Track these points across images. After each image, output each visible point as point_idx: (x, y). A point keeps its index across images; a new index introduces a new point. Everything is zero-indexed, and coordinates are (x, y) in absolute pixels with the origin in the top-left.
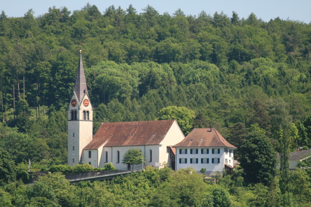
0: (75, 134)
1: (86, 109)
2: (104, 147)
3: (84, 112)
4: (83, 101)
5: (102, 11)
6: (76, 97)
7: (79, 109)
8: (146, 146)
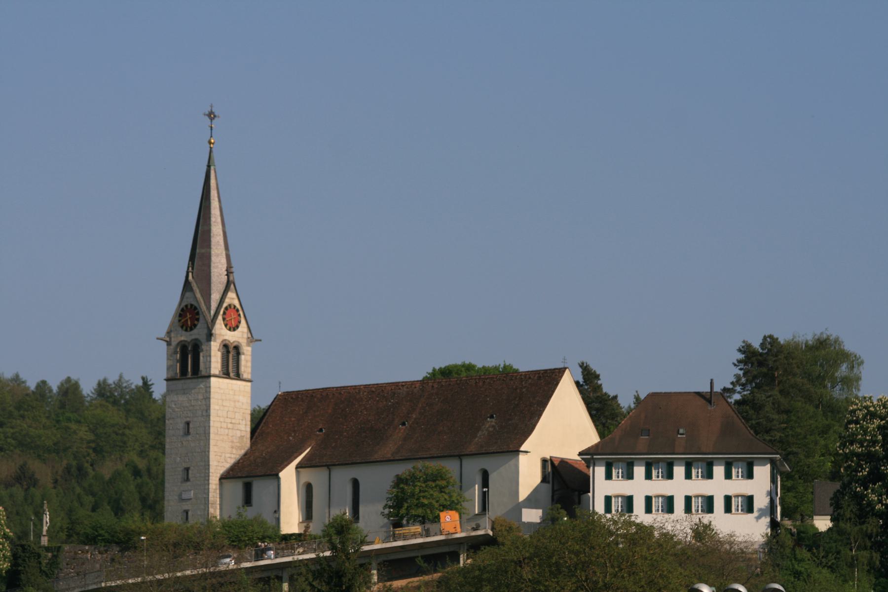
0: (191, 426)
1: (232, 337)
2: (298, 467)
3: (226, 346)
4: (222, 312)
5: (88, 388)
6: (198, 295)
7: (210, 336)
8: (462, 457)
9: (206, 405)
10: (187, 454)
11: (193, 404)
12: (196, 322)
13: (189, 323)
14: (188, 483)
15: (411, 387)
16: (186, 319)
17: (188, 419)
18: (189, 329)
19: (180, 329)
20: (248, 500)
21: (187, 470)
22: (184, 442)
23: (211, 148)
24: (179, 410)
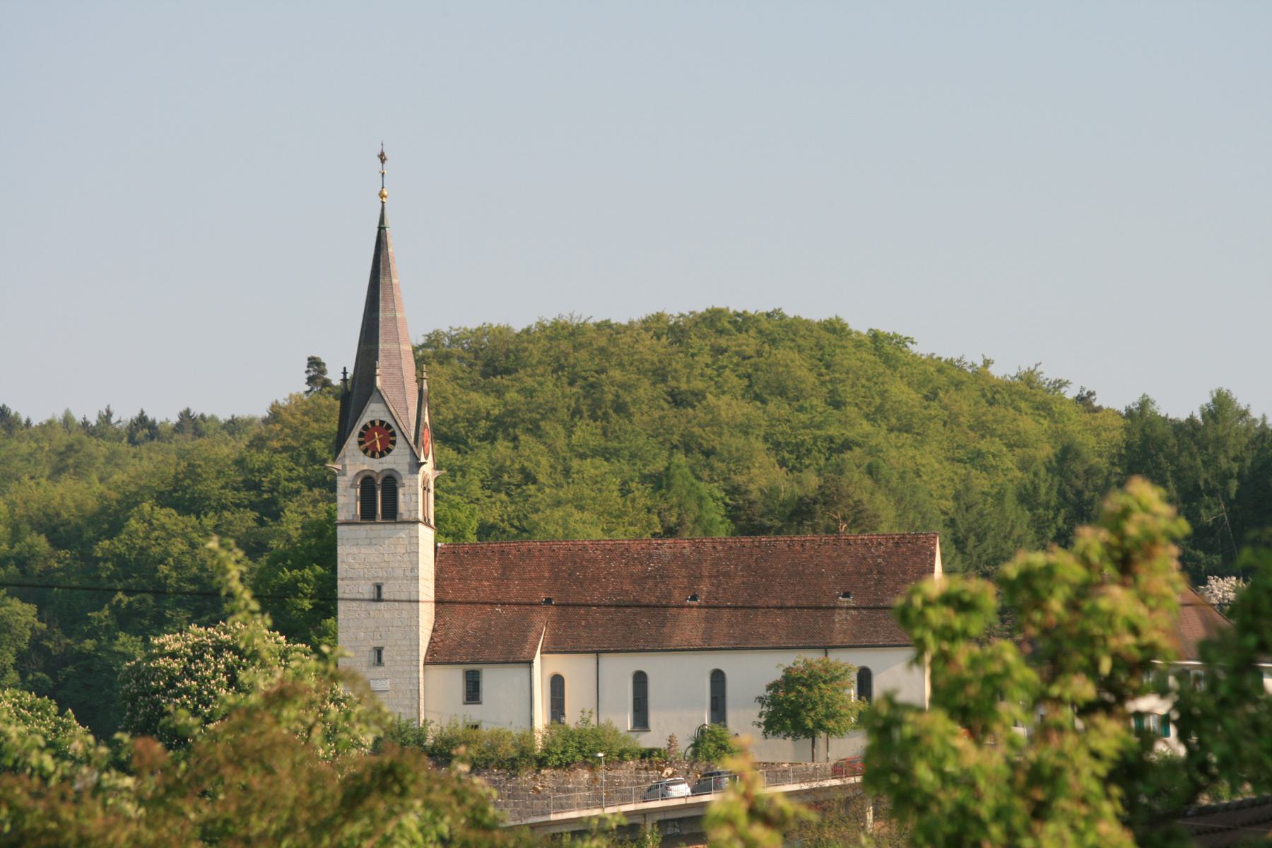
9: (411, 562)
10: (378, 627)
11: (387, 560)
12: (390, 446)
13: (379, 446)
14: (381, 669)
15: (675, 546)
16: (373, 441)
17: (378, 581)
18: (377, 455)
19: (362, 454)
20: (473, 693)
21: (379, 651)
22: (371, 612)
23: (383, 203)
24: (362, 567)
